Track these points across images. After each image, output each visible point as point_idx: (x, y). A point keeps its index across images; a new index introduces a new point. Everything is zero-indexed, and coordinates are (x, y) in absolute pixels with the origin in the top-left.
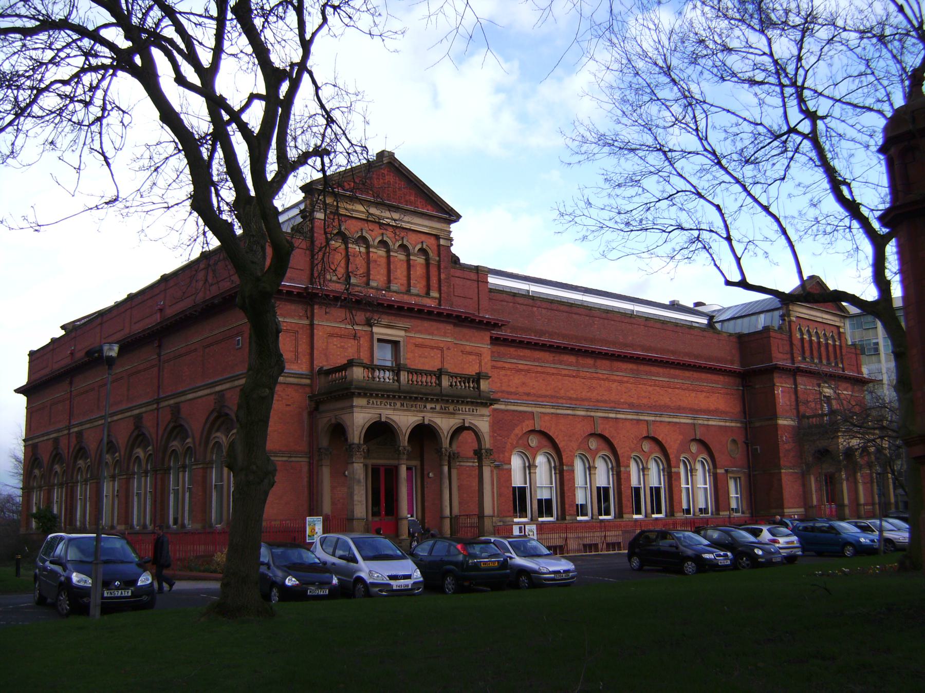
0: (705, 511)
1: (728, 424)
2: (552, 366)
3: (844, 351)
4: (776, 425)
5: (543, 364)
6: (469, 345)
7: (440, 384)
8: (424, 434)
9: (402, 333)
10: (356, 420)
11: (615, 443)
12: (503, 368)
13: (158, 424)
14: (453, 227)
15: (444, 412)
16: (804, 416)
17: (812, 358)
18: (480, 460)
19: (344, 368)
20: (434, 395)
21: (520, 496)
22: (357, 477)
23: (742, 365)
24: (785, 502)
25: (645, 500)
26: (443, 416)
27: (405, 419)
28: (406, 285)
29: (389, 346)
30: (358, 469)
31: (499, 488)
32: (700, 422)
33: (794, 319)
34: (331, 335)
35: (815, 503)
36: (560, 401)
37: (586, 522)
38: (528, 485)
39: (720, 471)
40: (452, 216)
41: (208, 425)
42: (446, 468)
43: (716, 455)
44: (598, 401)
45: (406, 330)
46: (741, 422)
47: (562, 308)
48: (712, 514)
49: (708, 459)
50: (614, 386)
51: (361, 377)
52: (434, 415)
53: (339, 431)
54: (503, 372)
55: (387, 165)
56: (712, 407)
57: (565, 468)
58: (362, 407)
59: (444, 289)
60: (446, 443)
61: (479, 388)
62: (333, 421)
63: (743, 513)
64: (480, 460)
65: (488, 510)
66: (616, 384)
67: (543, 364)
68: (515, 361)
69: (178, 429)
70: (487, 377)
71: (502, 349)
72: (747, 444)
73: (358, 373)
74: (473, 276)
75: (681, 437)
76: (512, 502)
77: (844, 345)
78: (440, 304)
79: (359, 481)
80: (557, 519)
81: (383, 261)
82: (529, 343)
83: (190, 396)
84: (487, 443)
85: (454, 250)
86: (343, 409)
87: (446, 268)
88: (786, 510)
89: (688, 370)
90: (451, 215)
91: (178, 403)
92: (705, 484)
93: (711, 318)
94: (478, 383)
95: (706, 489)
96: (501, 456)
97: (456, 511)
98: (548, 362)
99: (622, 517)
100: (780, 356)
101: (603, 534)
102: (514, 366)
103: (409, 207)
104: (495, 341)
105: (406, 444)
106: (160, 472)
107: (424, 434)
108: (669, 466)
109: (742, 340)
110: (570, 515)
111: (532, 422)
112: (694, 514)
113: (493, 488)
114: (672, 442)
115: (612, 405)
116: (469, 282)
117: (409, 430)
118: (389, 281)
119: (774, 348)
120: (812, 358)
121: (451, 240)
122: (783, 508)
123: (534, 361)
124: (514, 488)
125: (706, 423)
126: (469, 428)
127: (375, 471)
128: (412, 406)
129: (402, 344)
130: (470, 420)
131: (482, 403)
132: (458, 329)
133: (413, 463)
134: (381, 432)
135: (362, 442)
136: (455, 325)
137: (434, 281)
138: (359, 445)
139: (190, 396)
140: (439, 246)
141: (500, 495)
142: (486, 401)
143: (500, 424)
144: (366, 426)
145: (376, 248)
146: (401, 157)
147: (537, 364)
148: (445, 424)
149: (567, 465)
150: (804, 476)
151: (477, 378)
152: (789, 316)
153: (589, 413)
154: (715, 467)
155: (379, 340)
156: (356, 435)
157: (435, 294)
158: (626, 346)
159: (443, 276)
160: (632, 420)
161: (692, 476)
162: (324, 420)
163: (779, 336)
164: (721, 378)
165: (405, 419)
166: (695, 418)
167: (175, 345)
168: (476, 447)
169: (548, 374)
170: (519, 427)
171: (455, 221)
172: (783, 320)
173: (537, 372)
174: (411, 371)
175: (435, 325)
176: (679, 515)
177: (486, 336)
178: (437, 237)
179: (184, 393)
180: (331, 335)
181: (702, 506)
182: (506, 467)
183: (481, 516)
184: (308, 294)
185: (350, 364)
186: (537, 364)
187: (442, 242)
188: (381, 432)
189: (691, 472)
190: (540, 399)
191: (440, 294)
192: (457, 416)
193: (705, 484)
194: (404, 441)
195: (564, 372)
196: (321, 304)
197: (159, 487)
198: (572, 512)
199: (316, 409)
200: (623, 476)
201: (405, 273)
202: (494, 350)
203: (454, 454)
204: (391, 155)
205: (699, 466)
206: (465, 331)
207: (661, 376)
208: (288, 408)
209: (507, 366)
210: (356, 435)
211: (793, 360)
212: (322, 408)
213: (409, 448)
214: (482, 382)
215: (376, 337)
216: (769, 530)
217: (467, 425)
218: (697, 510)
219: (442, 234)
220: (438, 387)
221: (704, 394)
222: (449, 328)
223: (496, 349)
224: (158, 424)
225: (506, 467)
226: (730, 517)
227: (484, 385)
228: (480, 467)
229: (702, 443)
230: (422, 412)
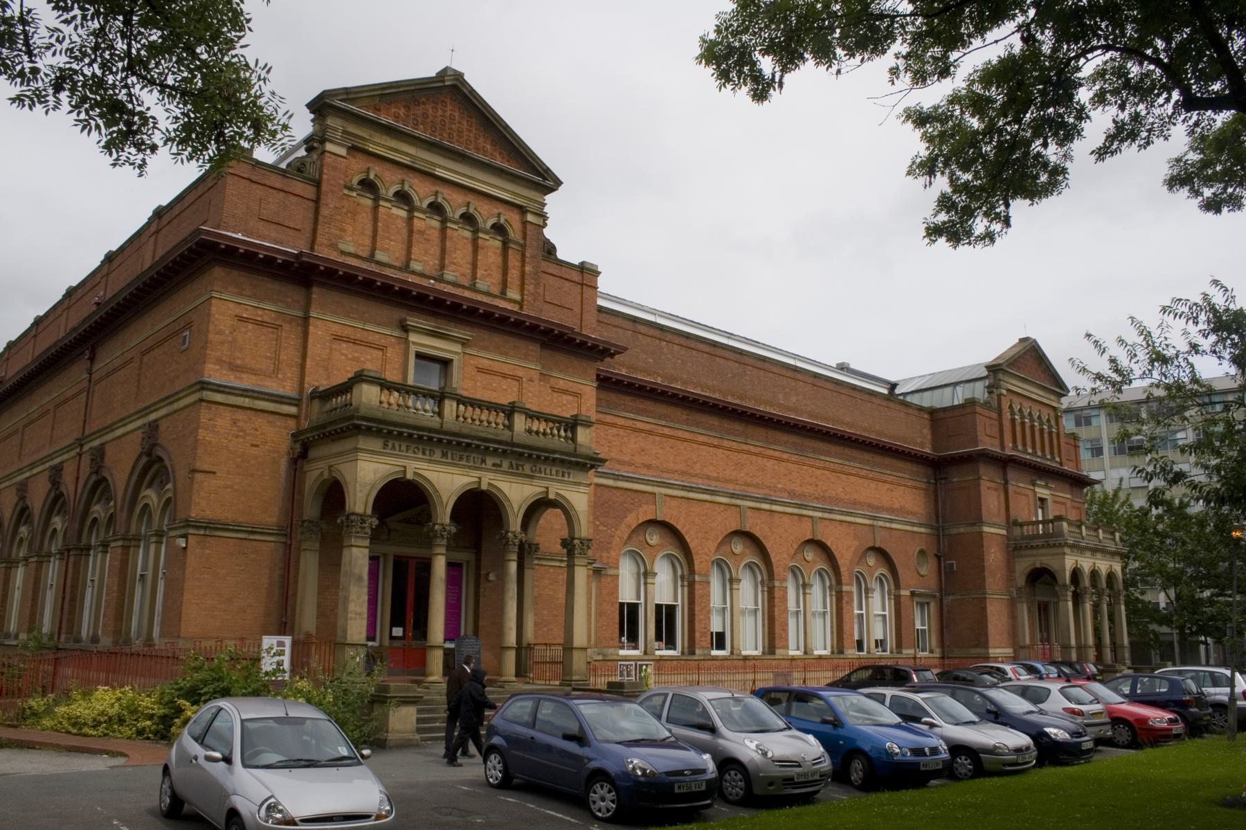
0: (880, 644)
1: (915, 529)
2: (685, 427)
3: (1062, 440)
4: (981, 533)
5: (671, 424)
6: (563, 379)
7: (510, 427)
8: (478, 509)
9: (457, 348)
10: (360, 474)
11: (768, 546)
12: (613, 425)
13: (78, 478)
14: (549, 198)
15: (515, 472)
16: (1016, 523)
17: (1024, 445)
18: (571, 554)
19: (345, 388)
20: (500, 442)
21: (629, 618)
22: (357, 571)
23: (934, 447)
24: (991, 638)
25: (647, 625)
26: (514, 479)
27: (448, 481)
28: (469, 277)
29: (437, 366)
30: (358, 557)
31: (599, 604)
32: (881, 523)
33: (1004, 392)
34: (338, 338)
35: (1028, 641)
36: (694, 480)
37: (724, 659)
38: (642, 601)
39: (905, 593)
40: (545, 181)
41: (135, 478)
42: (513, 567)
43: (900, 571)
44: (747, 485)
45: (464, 343)
46: (931, 527)
47: (701, 347)
48: (891, 652)
49: (889, 576)
50: (770, 464)
51: (375, 402)
52: (499, 477)
53: (334, 494)
54: (614, 431)
55: (450, 90)
56: (897, 505)
57: (697, 578)
58: (373, 452)
59: (530, 288)
60: (515, 524)
61: (574, 439)
62: (326, 475)
63: (931, 651)
64: (571, 554)
65: (579, 639)
66: (772, 462)
67: (671, 424)
68: (632, 416)
69: (99, 487)
70: (588, 424)
71: (613, 397)
72: (938, 557)
73: (369, 395)
74: (576, 276)
75: (856, 543)
76: (617, 626)
77: (1062, 433)
78: (521, 308)
79: (360, 578)
80: (683, 653)
81: (435, 235)
82: (653, 391)
83: (119, 432)
84: (584, 529)
85: (547, 232)
86: (341, 454)
87: (533, 257)
88: (991, 651)
89: (869, 451)
90: (545, 179)
91: (103, 445)
92: (884, 610)
93: (893, 386)
94: (574, 433)
95: (884, 616)
96: (605, 554)
97: (530, 635)
98: (679, 422)
99: (774, 653)
100: (987, 439)
101: (750, 676)
102: (629, 423)
103: (480, 157)
104: (607, 383)
105: (447, 520)
106: (76, 551)
107: (478, 509)
108: (839, 583)
109: (935, 416)
110: (702, 647)
111: (652, 507)
112: (869, 652)
113: (589, 603)
114: (845, 550)
115: (767, 491)
116: (567, 284)
117: (454, 498)
118: (442, 267)
119: (980, 429)
120: (1024, 445)
121: (544, 217)
122: (987, 647)
123: (660, 418)
124: (622, 605)
125: (888, 525)
126: (554, 504)
127: (400, 565)
128: (461, 458)
129: (455, 364)
130: (556, 489)
131: (578, 463)
132: (547, 353)
133: (461, 556)
134: (401, 499)
135: (369, 511)
136: (544, 346)
137: (514, 274)
138: (363, 518)
139: (119, 432)
140: (525, 223)
141: (600, 614)
142: (588, 463)
143: (602, 505)
144: (379, 487)
145: (423, 212)
146: (478, 81)
147: (663, 423)
148: (516, 492)
149: (700, 574)
150: (1012, 603)
151: (572, 425)
152: (998, 387)
153: (734, 501)
154: (898, 586)
155: (419, 356)
156: (360, 500)
157: (513, 294)
158: (789, 409)
159: (527, 268)
160: (792, 514)
161: (867, 598)
162: (315, 473)
163: (987, 413)
164: (908, 466)
165: (448, 481)
166: (874, 518)
167: (111, 354)
168: (565, 534)
169: (678, 439)
170: (633, 515)
171: (551, 190)
172: (990, 393)
173: (663, 435)
174: (461, 400)
175: (512, 342)
176: (852, 652)
177: (593, 368)
178: (522, 210)
179: (110, 428)
180: (338, 338)
181: (880, 636)
182: (611, 572)
183: (568, 648)
184: (303, 264)
185: (360, 378)
186: (663, 423)
187: (530, 218)
188: (401, 499)
189: (867, 593)
190: (665, 475)
191: (522, 295)
192: (536, 482)
193: (884, 610)
194: (444, 515)
195: (701, 438)
196: (322, 285)
197: (70, 575)
198: (704, 644)
199: (304, 455)
200: (777, 594)
201: (469, 259)
202: (601, 396)
203: (530, 546)
204: (459, 76)
205: (875, 585)
206: (559, 357)
207: (833, 458)
208: (254, 451)
209: (620, 421)
210: (360, 500)
211: (1003, 446)
212: (312, 454)
213: (453, 530)
214: (580, 430)
215: (413, 349)
216: (1062, 691)
217: (552, 496)
218: (873, 645)
219: (531, 206)
220: (507, 432)
221: (887, 486)
222: (534, 348)
223: (604, 395)
224: (78, 478)
225: (611, 572)
226: (915, 658)
227: (583, 435)
228: (571, 567)
229: (882, 553)
230: (477, 469)
